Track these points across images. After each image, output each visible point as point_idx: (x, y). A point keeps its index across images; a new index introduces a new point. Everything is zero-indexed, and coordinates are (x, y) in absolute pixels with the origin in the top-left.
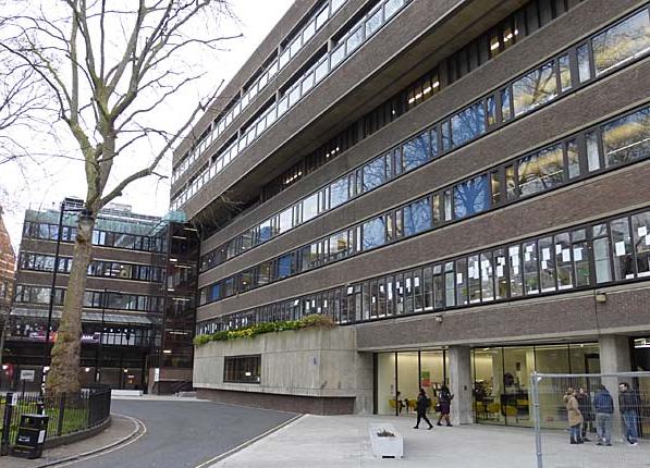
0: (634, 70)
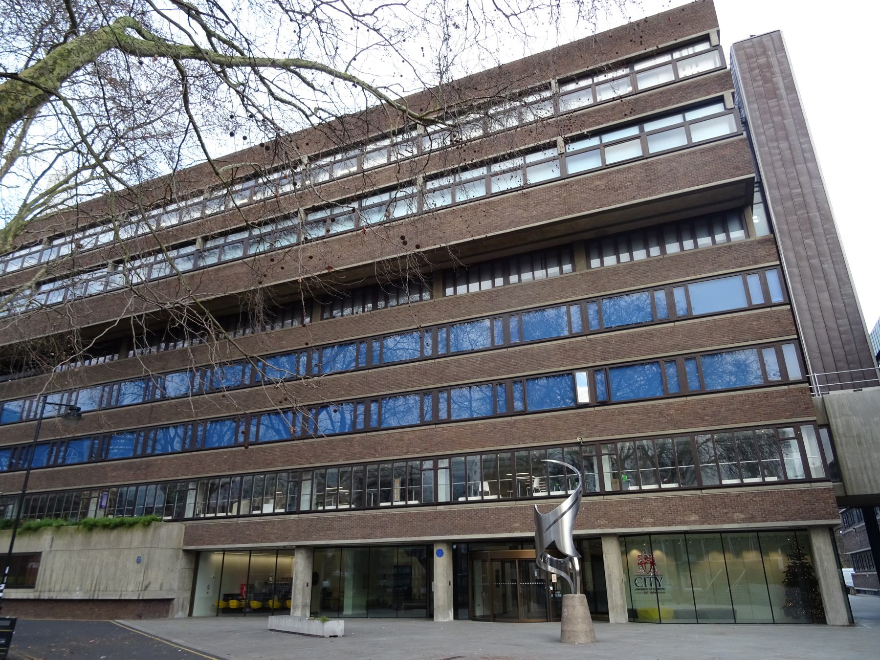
0: (477, 357)
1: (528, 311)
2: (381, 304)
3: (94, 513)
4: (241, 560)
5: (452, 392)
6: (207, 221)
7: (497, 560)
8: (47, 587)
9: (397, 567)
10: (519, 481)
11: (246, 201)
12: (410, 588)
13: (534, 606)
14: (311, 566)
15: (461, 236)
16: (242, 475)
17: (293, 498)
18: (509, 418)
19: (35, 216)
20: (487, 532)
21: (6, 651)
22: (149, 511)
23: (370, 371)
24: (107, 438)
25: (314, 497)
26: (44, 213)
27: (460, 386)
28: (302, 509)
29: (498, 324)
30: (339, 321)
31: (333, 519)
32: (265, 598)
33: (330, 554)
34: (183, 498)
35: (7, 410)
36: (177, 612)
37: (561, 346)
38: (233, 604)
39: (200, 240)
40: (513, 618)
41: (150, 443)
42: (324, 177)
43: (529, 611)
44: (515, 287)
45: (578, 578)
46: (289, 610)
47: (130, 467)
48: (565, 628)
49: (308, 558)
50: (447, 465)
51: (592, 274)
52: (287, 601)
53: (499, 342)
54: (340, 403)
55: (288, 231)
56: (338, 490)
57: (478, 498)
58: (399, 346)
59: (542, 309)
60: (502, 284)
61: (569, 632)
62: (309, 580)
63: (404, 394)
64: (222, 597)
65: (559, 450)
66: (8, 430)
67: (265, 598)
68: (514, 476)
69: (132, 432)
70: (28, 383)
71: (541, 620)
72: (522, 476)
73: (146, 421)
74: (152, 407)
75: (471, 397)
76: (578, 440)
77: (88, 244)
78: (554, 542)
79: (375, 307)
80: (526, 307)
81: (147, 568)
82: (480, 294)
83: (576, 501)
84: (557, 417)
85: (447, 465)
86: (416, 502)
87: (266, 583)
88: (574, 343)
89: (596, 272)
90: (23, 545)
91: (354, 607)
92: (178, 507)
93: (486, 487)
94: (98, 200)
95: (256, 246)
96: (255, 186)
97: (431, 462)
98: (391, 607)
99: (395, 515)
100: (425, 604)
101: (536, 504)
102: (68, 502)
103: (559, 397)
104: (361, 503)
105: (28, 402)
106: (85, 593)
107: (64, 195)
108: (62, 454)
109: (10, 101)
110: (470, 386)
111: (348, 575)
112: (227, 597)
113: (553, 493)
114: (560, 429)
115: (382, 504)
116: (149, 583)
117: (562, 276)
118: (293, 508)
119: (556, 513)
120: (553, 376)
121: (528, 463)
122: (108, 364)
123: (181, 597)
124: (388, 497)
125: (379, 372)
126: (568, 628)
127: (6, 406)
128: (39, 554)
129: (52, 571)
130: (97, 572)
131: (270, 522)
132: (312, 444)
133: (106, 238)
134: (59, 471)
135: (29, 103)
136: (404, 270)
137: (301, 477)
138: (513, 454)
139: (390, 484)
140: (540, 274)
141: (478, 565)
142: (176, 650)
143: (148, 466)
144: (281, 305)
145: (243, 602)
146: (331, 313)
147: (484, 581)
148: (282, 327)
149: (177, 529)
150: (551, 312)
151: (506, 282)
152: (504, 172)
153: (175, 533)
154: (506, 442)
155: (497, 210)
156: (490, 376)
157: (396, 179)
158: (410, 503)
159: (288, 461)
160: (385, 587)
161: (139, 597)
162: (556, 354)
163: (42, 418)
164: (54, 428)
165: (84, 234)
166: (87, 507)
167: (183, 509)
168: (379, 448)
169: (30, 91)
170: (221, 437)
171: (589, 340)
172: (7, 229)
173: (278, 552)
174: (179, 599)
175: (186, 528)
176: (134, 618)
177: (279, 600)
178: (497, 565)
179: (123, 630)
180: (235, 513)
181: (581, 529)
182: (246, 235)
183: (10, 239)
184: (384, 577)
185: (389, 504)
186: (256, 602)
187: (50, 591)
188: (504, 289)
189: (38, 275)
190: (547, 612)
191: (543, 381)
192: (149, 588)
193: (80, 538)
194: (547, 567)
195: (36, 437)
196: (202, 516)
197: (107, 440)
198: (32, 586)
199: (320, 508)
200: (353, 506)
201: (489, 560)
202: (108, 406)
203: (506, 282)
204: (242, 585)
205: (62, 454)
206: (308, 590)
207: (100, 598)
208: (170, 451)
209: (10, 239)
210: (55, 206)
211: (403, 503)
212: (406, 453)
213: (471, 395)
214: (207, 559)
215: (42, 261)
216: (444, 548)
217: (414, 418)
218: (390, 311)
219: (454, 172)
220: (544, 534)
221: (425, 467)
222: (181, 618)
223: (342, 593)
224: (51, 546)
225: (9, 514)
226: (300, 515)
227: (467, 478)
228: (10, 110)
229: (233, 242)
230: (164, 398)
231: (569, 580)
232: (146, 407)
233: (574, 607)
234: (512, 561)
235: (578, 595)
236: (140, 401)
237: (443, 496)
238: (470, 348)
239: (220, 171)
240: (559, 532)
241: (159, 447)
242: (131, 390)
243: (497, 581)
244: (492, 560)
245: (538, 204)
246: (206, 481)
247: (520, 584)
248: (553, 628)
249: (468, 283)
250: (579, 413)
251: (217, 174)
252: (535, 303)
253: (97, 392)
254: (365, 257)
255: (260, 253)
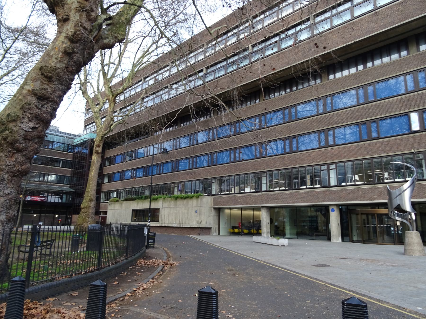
0: (349, 110)
1: (378, 82)
2: (294, 88)
3: (177, 193)
4: (238, 212)
5: (335, 130)
6: (208, 59)
7: (364, 214)
8: (163, 222)
9: (311, 217)
10: (376, 174)
11: (223, 46)
12: (317, 227)
13: (386, 237)
14: (269, 215)
15: (337, 45)
16: (234, 176)
17: (258, 186)
18: (369, 142)
19: (138, 68)
20: (358, 200)
21: (154, 245)
22: (198, 192)
23: (291, 123)
24: (178, 162)
25: (268, 184)
26: (141, 67)
27: (339, 127)
28: (331, 185)
29: (361, 92)
30: (273, 100)
31: (278, 194)
32: (250, 229)
33: (276, 210)
34: (211, 186)
35: (139, 152)
36: (214, 233)
37: (400, 99)
38: (236, 230)
39: (205, 70)
40: (375, 242)
41: (194, 163)
42: (260, 27)
43: (383, 239)
44: (371, 69)
45: (415, 224)
46: (261, 234)
47: (188, 173)
48: (407, 248)
49: (268, 212)
50: (335, 168)
51: (421, 54)
52: (260, 230)
53: (361, 101)
54: (275, 141)
55: (245, 58)
56: (279, 181)
57: (353, 183)
58: (304, 109)
59: (387, 80)
60: (320, 82)
61: (409, 250)
62: (269, 221)
63: (309, 134)
64: (231, 228)
65: (401, 157)
66: (141, 160)
67: (250, 229)
68: (373, 172)
69: (187, 159)
70: (146, 141)
71: (392, 244)
72: (377, 172)
73: (192, 154)
74: (194, 147)
75: (345, 133)
76: (412, 151)
77: (160, 78)
78: (399, 205)
79: (291, 91)
80: (377, 80)
81: (200, 215)
82: (349, 76)
83: (413, 183)
84: (399, 139)
85: (335, 168)
86: (319, 186)
87: (249, 222)
88: (409, 97)
89: (424, 53)
90: (154, 206)
91: (290, 234)
92: (209, 190)
93: (357, 178)
94: (160, 57)
95: (231, 67)
96: (227, 38)
97: (326, 167)
98: (308, 235)
99: (309, 192)
100: (326, 234)
101: (388, 186)
102: (166, 189)
103: (398, 129)
104: (291, 187)
105: (146, 149)
106: (178, 224)
107: (148, 57)
108: (161, 168)
109: (125, 15)
110: (344, 126)
111: (287, 220)
112: (234, 228)
113: (396, 180)
114: (400, 146)
115: (301, 187)
116: (201, 221)
117: (401, 59)
118: (259, 189)
119: (401, 190)
120: (395, 117)
121: (381, 165)
122: (174, 130)
123: (215, 227)
124: (304, 183)
125: (295, 123)
126: (409, 248)
127: (138, 151)
128: (159, 209)
129: (164, 215)
130: (181, 216)
131: (249, 196)
132: (265, 160)
133: (166, 74)
134: (161, 176)
135: (132, 15)
136: (308, 68)
137: (261, 176)
138: (372, 161)
139: (305, 177)
140: (386, 60)
141: (354, 217)
142: (216, 248)
143: (195, 173)
144: (246, 94)
145: (240, 230)
146: (269, 96)
147: (358, 224)
148: (246, 106)
149: (210, 198)
150: (392, 81)
151: (365, 67)
152: (323, 21)
153: (209, 201)
154: (367, 154)
155: (358, 26)
156: (357, 120)
157: (255, 40)
158: (315, 186)
159: (254, 168)
160: (304, 226)
161: (198, 226)
162: (397, 104)
163: (153, 155)
164: (158, 159)
165: (227, 35)
166: (174, 191)
167: (211, 191)
168: (298, 161)
169: (132, 9)
170: (223, 159)
171: (419, 94)
172: (129, 76)
173: (253, 209)
174: (214, 228)
175: (213, 198)
176: (197, 235)
177: (256, 229)
178: (364, 217)
179: (194, 239)
180: (233, 192)
181: (414, 198)
182: (225, 63)
183: (131, 80)
184: (304, 221)
185: (305, 187)
186: (246, 230)
187: (165, 223)
188: (364, 71)
189: (142, 95)
190: (394, 240)
191: (388, 121)
192: (202, 223)
193: (173, 203)
194: (395, 218)
195: (153, 162)
196: (219, 193)
197: (177, 163)
198: (158, 221)
199: (271, 189)
200: (287, 188)
201: (360, 214)
202: (177, 148)
203: (365, 67)
204: (239, 223)
205: (161, 168)
206: (269, 226)
207: (183, 226)
208: (202, 166)
209: (131, 80)
210: (145, 63)
211: (312, 186)
212: (312, 163)
213: (345, 131)
214: (223, 211)
215: (143, 88)
216: (335, 208)
217: (315, 145)
218: (299, 91)
219: (334, 7)
220: (393, 201)
221: (322, 169)
222: (215, 236)
223: (284, 228)
224: (163, 206)
225: (146, 194)
226: (262, 193)
227: (345, 174)
228: (126, 19)
229: (219, 68)
230: (198, 144)
231: (409, 224)
232: (191, 148)
233: (412, 238)
234: (373, 215)
235: (415, 232)
236: (188, 145)
237: (333, 182)
238: (343, 107)
239: (212, 32)
240: (402, 200)
241: (198, 165)
242: (184, 142)
243: (364, 224)
244: (362, 214)
245: (384, 17)
246: (219, 179)
247: (378, 226)
248: (400, 248)
249: (342, 71)
250: (413, 136)
251: (211, 34)
252: (383, 76)
253: (171, 142)
254: (284, 65)
255: (234, 70)
